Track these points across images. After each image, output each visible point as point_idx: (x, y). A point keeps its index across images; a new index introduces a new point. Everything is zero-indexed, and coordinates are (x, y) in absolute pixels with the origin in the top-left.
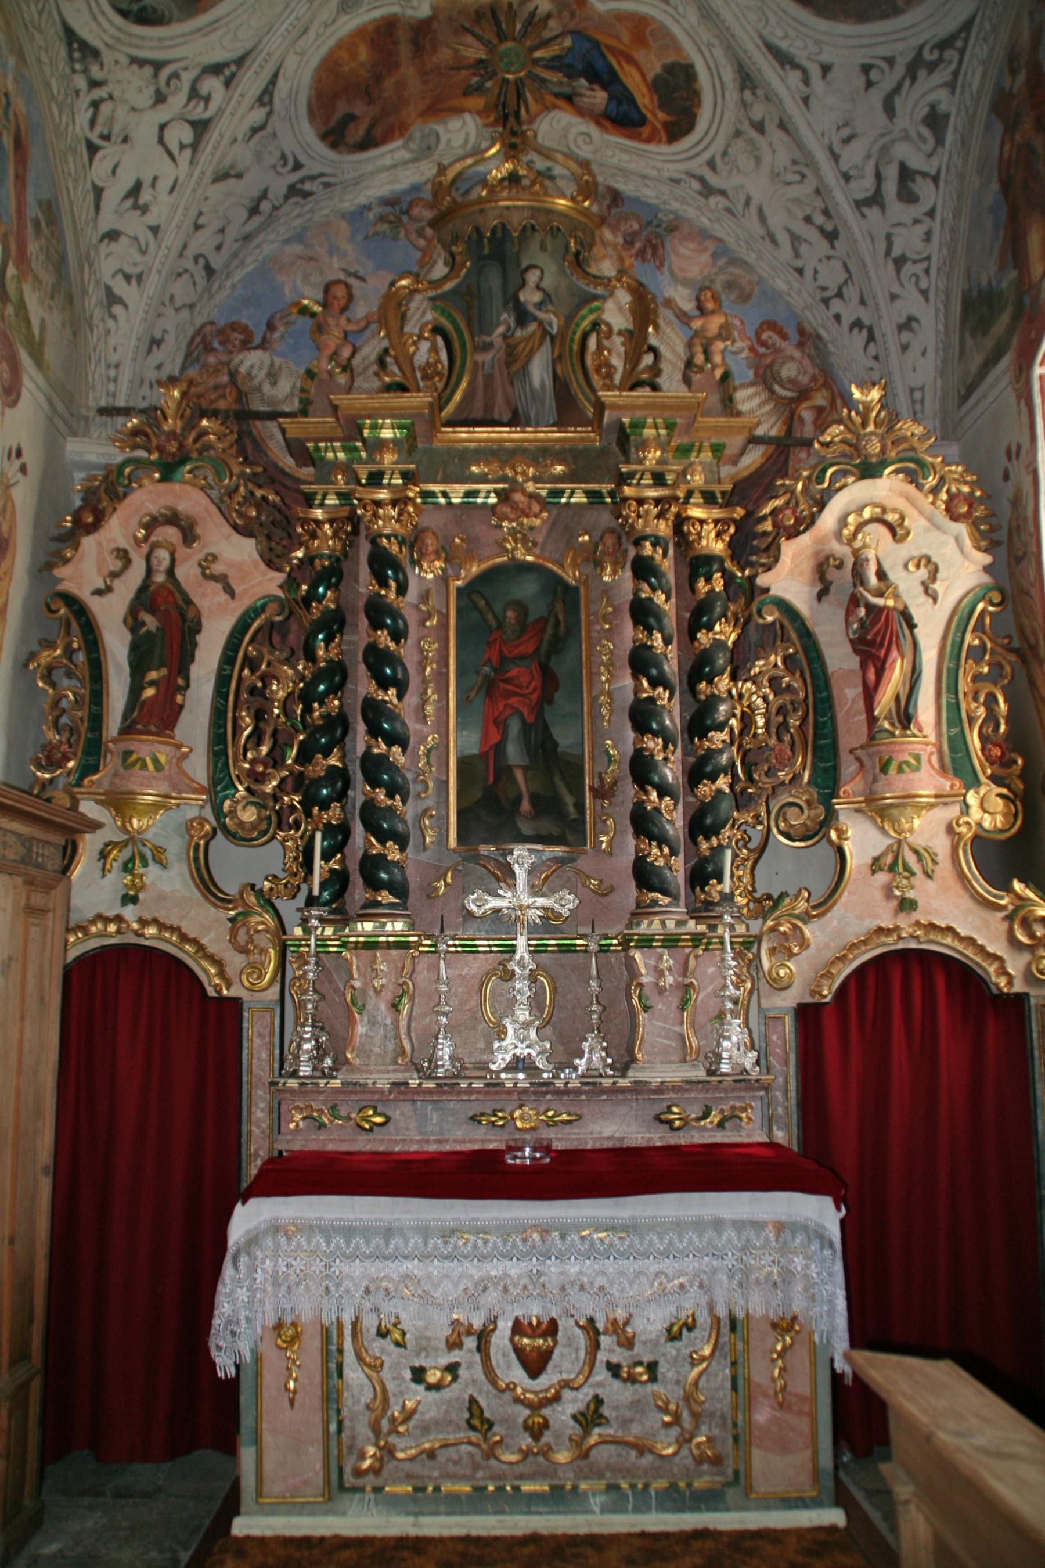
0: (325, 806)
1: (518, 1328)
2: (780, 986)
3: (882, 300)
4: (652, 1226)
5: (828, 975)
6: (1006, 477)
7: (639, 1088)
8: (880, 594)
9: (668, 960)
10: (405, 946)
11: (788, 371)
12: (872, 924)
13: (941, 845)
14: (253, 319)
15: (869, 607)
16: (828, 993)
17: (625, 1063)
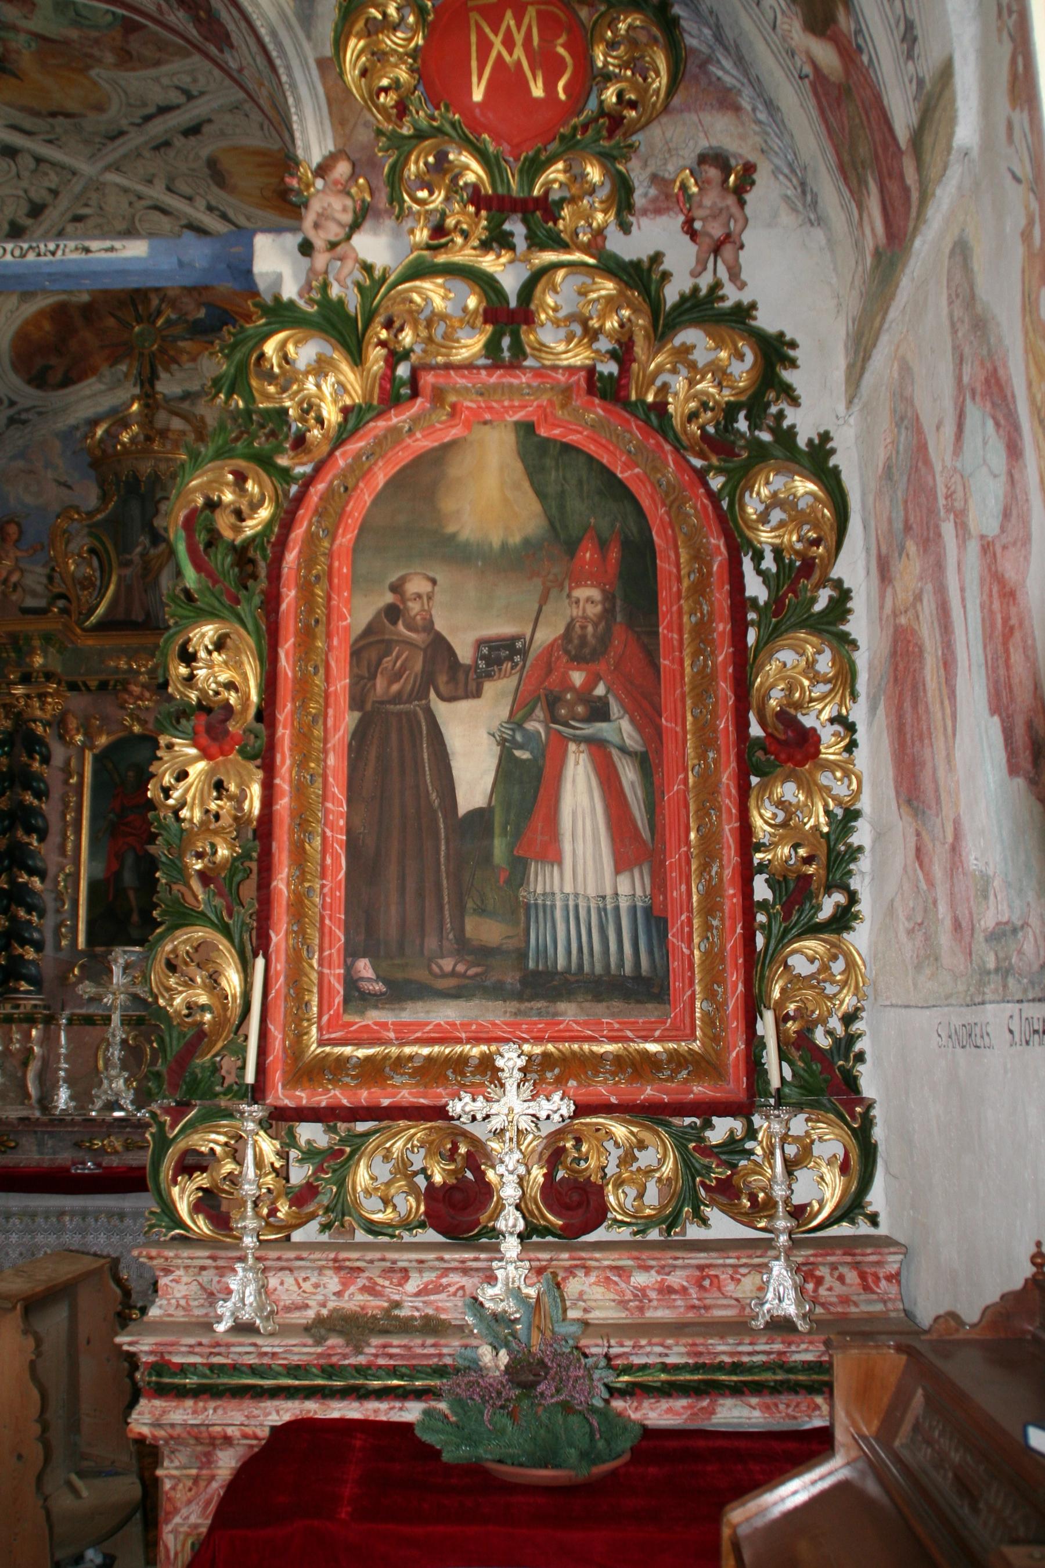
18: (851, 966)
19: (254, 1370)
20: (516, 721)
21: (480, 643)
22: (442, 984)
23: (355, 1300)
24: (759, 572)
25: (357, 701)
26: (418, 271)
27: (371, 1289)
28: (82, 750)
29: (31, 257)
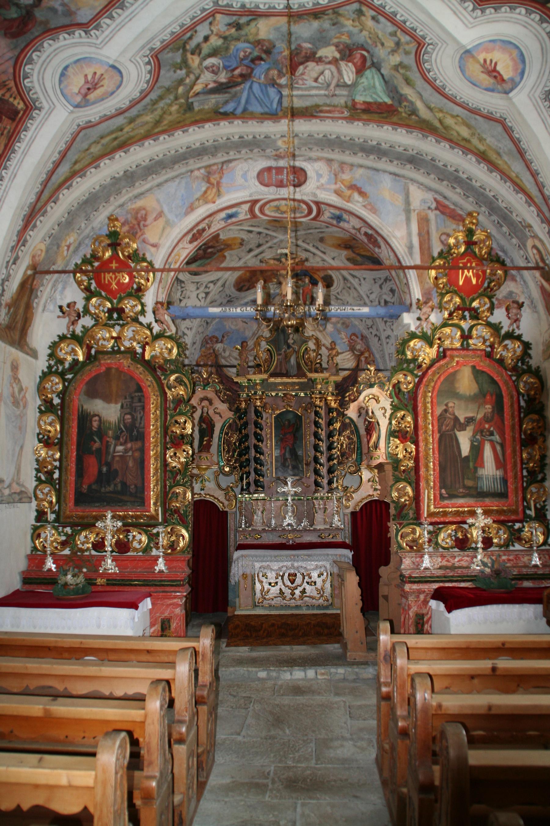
0: (245, 468)
1: (289, 575)
2: (347, 507)
3: (381, 330)
4: (315, 555)
5: (358, 505)
7: (315, 530)
9: (321, 502)
10: (265, 499)
11: (358, 347)
12: (368, 494)
14: (219, 335)
15: (369, 422)
16: (358, 509)
18: (545, 491)
19: (430, 577)
20: (474, 436)
21: (466, 418)
22: (460, 495)
23: (444, 563)
24: (524, 400)
25: (439, 431)
26: (445, 325)
27: (448, 561)
28: (271, 415)
29: (339, 311)
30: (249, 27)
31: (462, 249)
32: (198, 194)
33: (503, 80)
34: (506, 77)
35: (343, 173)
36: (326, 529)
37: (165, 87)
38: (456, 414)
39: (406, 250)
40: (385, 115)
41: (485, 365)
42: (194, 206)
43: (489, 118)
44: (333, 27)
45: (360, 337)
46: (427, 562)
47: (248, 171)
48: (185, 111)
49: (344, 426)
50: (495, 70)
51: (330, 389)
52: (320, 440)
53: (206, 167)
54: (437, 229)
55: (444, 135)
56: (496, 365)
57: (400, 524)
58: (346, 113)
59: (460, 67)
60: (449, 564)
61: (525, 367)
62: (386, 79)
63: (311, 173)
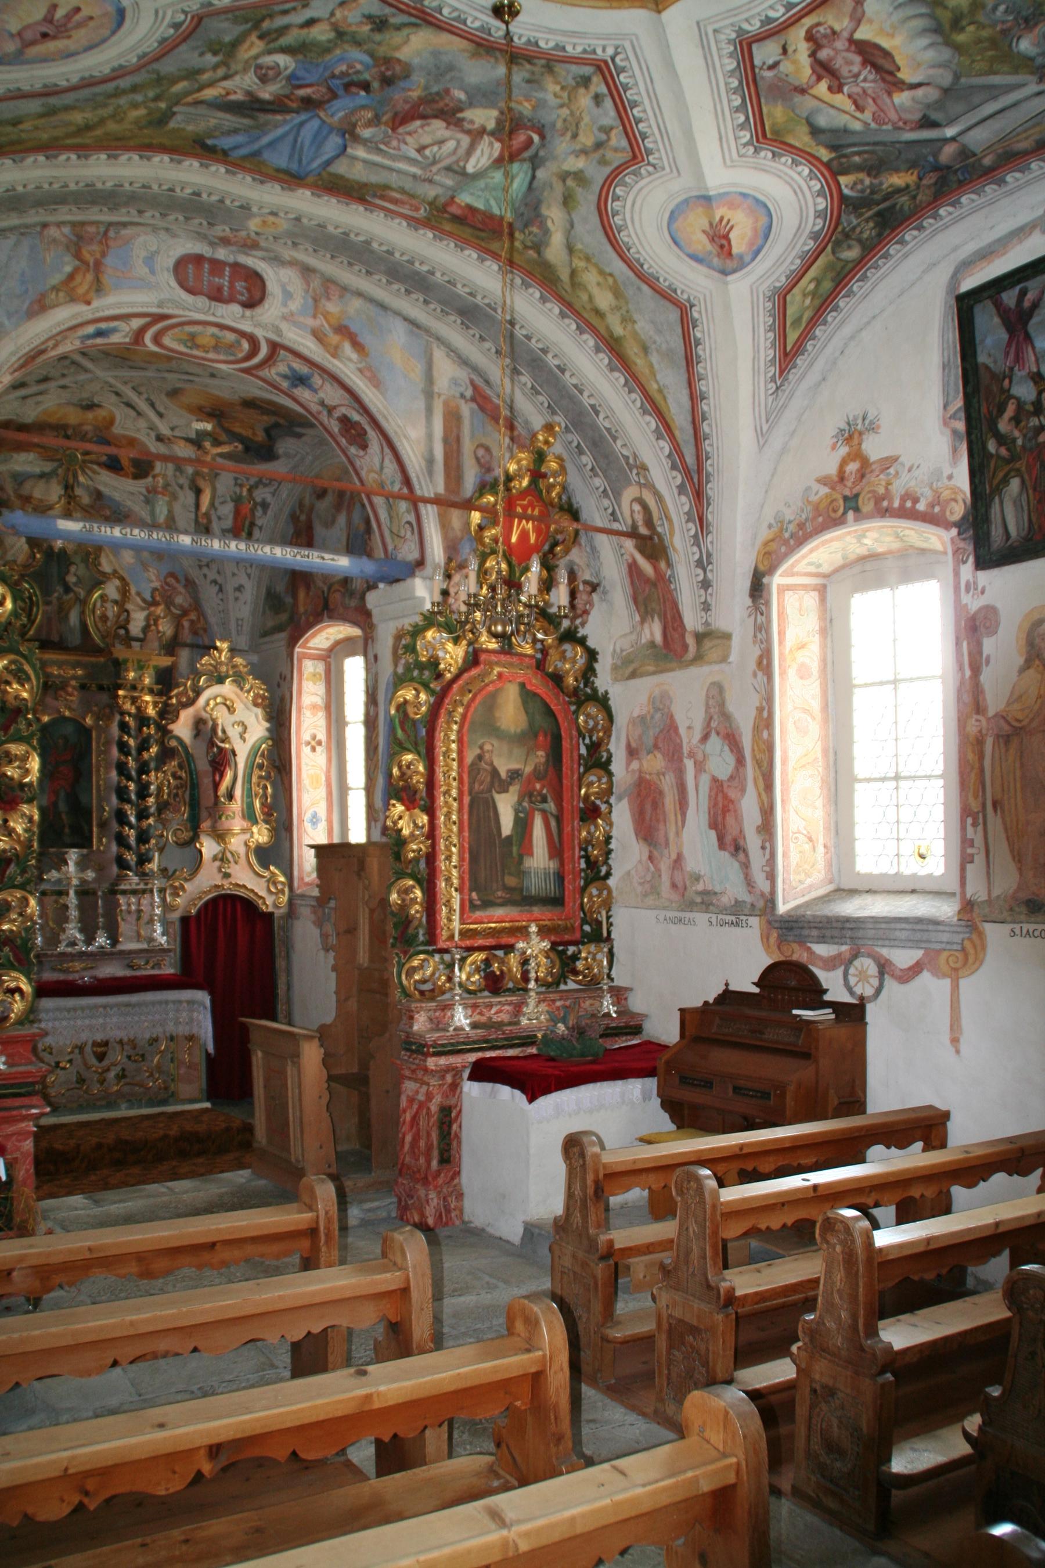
6: (279, 686)
8: (223, 741)
11: (179, 600)
13: (242, 850)
17: (115, 942)
20: (520, 802)
21: (509, 771)
22: (499, 901)
25: (470, 793)
27: (481, 1014)
29: (298, 557)
30: (395, 34)
31: (525, 483)
32: (56, 279)
33: (730, 254)
34: (735, 250)
35: (328, 299)
36: (142, 951)
37: (158, 74)
38: (496, 763)
39: (423, 464)
40: (483, 235)
41: (537, 683)
42: (47, 302)
43: (667, 296)
44: (524, 85)
45: (183, 582)
46: (461, 1018)
47: (157, 252)
48: (150, 123)
49: (166, 754)
50: (726, 237)
51: (147, 681)
52: (129, 778)
53: (74, 225)
54: (473, 436)
55: (567, 297)
56: (550, 683)
57: (405, 953)
58: (422, 211)
59: (672, 212)
60: (483, 1019)
61: (588, 690)
62: (535, 184)
63: (272, 286)
